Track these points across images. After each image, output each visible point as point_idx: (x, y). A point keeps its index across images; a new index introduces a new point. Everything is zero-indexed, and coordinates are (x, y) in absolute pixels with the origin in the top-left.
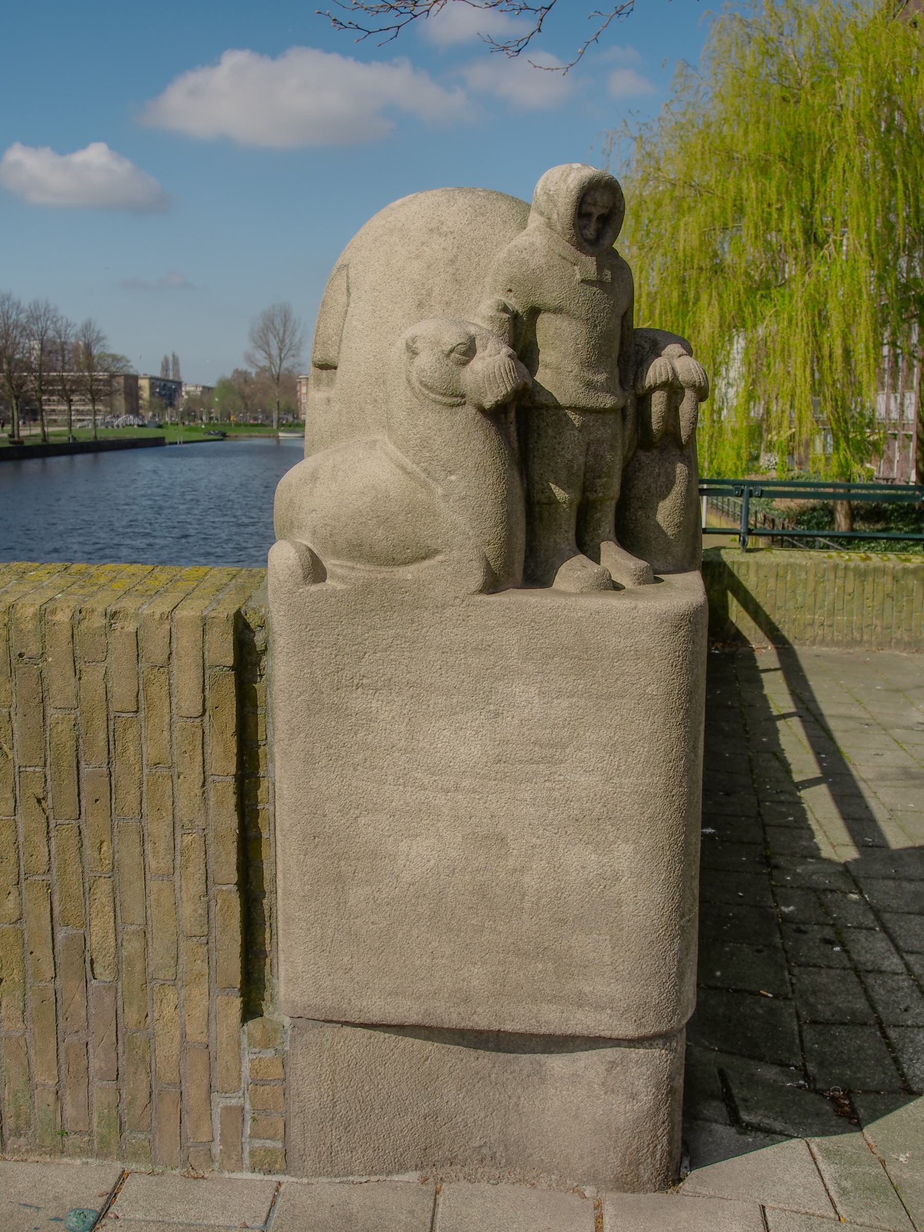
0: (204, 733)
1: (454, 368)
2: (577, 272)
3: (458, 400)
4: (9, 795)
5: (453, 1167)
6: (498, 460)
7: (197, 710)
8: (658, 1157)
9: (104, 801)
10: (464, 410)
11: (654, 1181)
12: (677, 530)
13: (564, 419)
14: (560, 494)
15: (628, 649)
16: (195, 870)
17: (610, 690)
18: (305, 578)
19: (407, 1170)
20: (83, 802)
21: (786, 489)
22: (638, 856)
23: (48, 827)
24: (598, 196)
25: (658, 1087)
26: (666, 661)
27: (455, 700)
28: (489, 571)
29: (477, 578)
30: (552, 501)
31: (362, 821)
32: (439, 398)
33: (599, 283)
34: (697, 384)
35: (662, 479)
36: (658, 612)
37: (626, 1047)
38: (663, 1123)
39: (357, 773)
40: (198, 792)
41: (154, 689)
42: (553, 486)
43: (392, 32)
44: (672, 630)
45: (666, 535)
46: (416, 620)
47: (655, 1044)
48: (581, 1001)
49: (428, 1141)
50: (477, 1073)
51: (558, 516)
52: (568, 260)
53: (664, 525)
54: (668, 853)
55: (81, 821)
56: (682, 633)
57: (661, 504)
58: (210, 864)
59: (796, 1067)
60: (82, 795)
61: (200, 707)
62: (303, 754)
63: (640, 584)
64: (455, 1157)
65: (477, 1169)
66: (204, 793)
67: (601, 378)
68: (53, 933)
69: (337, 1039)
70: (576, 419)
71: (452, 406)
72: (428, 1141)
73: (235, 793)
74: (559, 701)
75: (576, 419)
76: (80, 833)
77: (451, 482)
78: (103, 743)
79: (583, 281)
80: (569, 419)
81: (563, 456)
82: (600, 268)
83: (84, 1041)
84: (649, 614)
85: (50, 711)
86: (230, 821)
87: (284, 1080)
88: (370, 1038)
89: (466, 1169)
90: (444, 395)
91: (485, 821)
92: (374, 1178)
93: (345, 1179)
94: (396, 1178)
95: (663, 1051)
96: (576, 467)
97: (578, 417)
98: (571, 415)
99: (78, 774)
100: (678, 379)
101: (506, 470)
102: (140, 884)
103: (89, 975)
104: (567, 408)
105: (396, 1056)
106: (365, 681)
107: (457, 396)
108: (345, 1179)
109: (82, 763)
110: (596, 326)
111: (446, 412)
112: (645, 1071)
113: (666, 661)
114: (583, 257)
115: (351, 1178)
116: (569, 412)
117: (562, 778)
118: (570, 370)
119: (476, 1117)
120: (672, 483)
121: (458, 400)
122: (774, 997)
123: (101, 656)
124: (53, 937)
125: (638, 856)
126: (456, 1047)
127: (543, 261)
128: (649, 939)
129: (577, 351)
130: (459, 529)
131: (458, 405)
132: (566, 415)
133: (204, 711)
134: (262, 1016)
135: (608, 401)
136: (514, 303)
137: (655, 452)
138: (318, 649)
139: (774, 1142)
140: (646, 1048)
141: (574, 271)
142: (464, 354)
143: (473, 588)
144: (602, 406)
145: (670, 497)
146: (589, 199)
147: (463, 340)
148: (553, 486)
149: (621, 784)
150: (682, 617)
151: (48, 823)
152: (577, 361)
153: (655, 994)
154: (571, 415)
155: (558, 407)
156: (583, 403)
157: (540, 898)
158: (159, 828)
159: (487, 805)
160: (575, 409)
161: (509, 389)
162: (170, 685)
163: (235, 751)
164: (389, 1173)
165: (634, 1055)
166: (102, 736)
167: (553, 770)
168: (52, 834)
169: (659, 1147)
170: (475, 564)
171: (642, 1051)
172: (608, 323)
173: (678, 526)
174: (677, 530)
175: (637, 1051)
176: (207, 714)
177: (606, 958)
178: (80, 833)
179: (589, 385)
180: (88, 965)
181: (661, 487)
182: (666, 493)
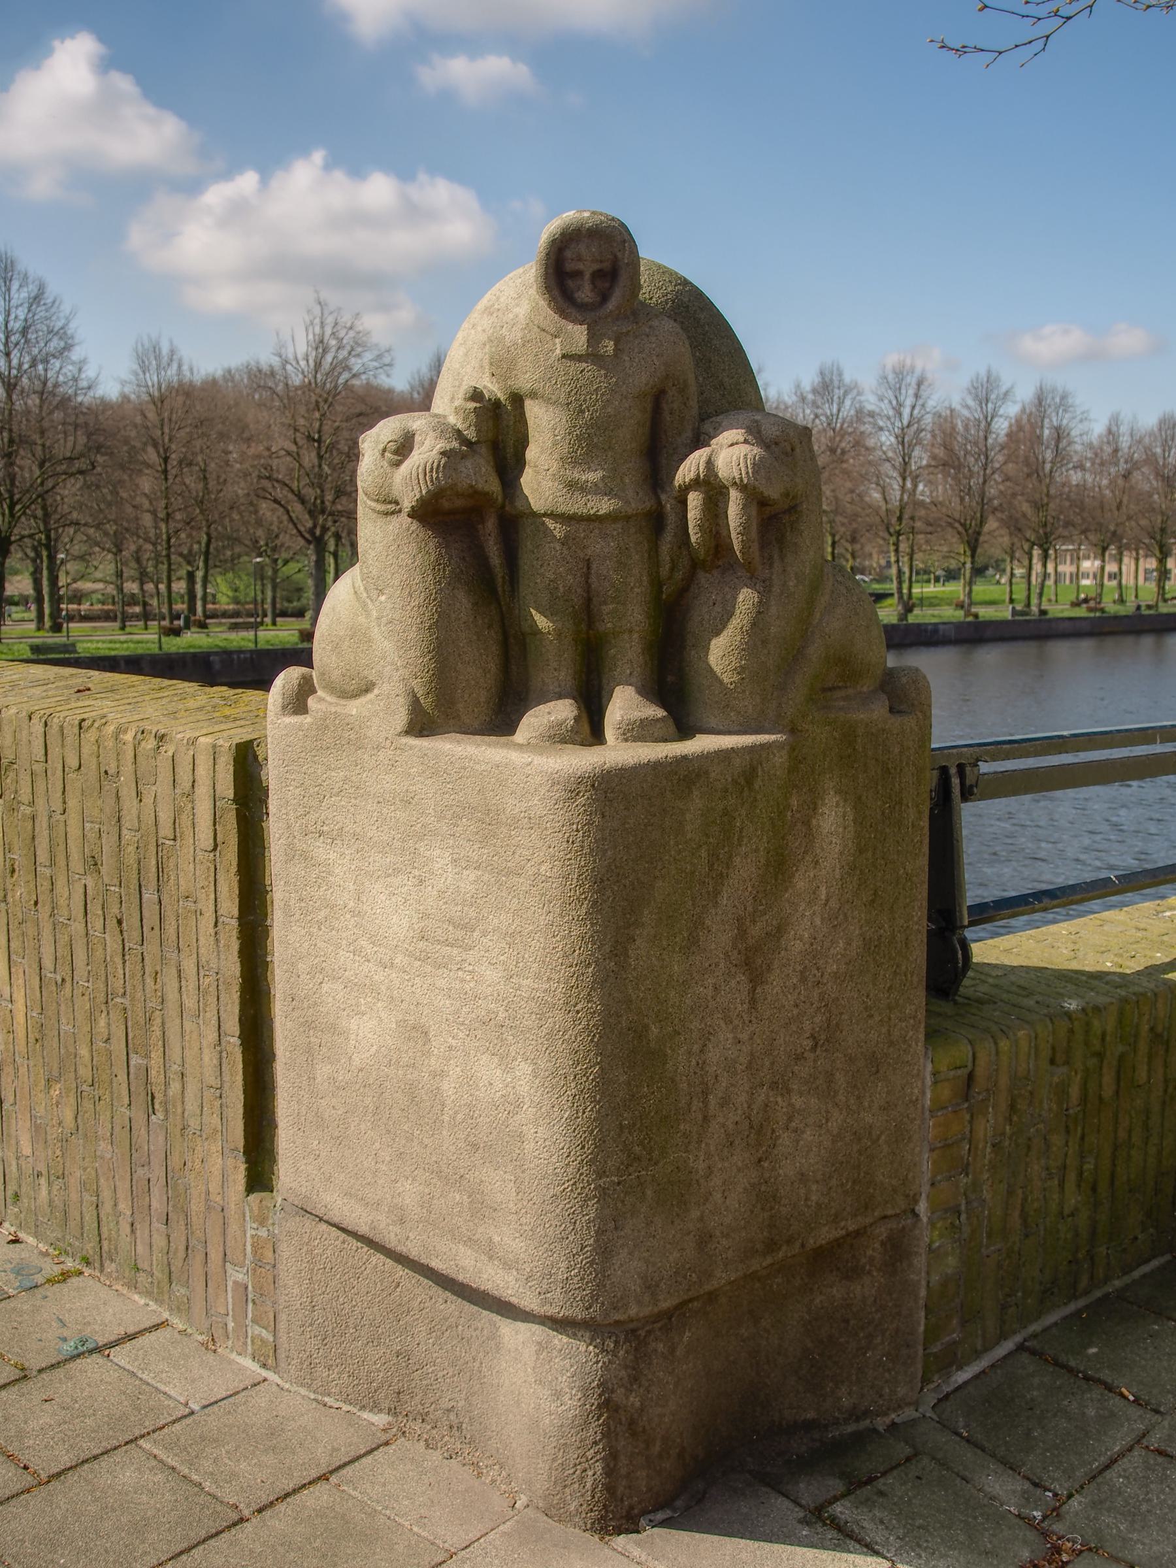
0: (216, 869)
1: (389, 470)
2: (558, 346)
3: (392, 507)
4: (100, 912)
5: (424, 1425)
6: (431, 577)
7: (209, 844)
8: (589, 1485)
9: (157, 928)
10: (400, 519)
11: (584, 1515)
12: (736, 678)
13: (542, 528)
14: (542, 622)
15: (522, 814)
16: (211, 1015)
17: (509, 864)
18: (284, 708)
19: (380, 1411)
20: (145, 929)
21: (45, 583)
22: (537, 1081)
23: (124, 949)
24: (582, 248)
25: (585, 1390)
26: (560, 835)
27: (388, 860)
28: (415, 706)
29: (401, 718)
30: (536, 632)
31: (325, 987)
32: (373, 504)
33: (592, 356)
34: (738, 481)
35: (718, 608)
36: (550, 770)
37: (549, 1328)
38: (595, 1443)
39: (321, 933)
40: (212, 931)
41: (184, 817)
42: (533, 612)
43: (1039, 45)
44: (566, 795)
45: (721, 682)
46: (359, 762)
47: (580, 1334)
48: (490, 1252)
49: (400, 1385)
50: (446, 1319)
51: (544, 650)
52: (547, 332)
53: (717, 669)
54: (573, 1085)
55: (144, 947)
56: (581, 800)
57: (713, 642)
58: (222, 1012)
59: (1056, 1495)
60: (144, 920)
61: (211, 841)
62: (283, 903)
63: (626, 740)
64: (427, 1413)
65: (444, 1436)
66: (216, 933)
67: (593, 476)
68: (128, 1059)
69: (314, 1234)
70: (556, 529)
71: (387, 514)
72: (400, 1385)
73: (238, 938)
74: (468, 872)
75: (556, 529)
76: (143, 959)
77: (381, 603)
78: (154, 870)
79: (564, 356)
80: (547, 527)
81: (543, 576)
82: (594, 338)
83: (147, 1177)
84: (541, 772)
85: (124, 832)
86: (232, 967)
87: (274, 1266)
88: (344, 1242)
89: (434, 1432)
90: (377, 501)
91: (412, 1007)
92: (346, 1408)
93: (320, 1398)
94: (365, 1415)
95: (591, 1348)
96: (562, 590)
97: (558, 526)
98: (550, 523)
99: (141, 899)
100: (716, 476)
101: (441, 589)
102: (178, 1021)
103: (150, 1110)
104: (545, 515)
105: (368, 1271)
106: (325, 828)
107: (390, 502)
108: (320, 1398)
109: (143, 888)
110: (583, 412)
111: (381, 521)
112: (568, 1366)
113: (560, 835)
114: (570, 326)
115: (326, 1399)
116: (546, 520)
117: (471, 968)
118: (546, 467)
119: (445, 1372)
120: (731, 614)
121: (392, 507)
122: (1134, 1401)
123: (152, 780)
124: (128, 1062)
125: (537, 1081)
126: (426, 1281)
127: (519, 335)
128: (552, 1192)
129: (555, 444)
130: (388, 659)
131: (393, 513)
132: (544, 523)
133: (216, 846)
134: (272, 1191)
135: (604, 506)
136: (493, 388)
137: (715, 572)
138: (291, 788)
139: (837, 1547)
140: (568, 1336)
141: (555, 344)
142: (396, 452)
143: (399, 729)
144: (592, 512)
145: (725, 633)
146: (568, 254)
147: (395, 437)
148: (533, 612)
149: (520, 986)
150: (580, 780)
151: (124, 945)
152: (556, 456)
153: (563, 1265)
154: (550, 523)
155: (534, 514)
156: (562, 509)
157: (456, 1113)
158: (189, 966)
159: (413, 989)
160: (552, 515)
161: (424, 492)
162: (194, 815)
163: (237, 892)
164: (363, 1408)
165: (556, 1341)
166: (154, 862)
167: (464, 957)
168: (127, 957)
169: (590, 1473)
170: (401, 700)
171: (565, 1339)
172: (604, 407)
173: (741, 670)
174: (736, 678)
175: (560, 1336)
176: (219, 848)
177: (511, 1205)
178: (143, 959)
179: (573, 486)
180: (150, 1098)
181: (715, 618)
182: (720, 627)
